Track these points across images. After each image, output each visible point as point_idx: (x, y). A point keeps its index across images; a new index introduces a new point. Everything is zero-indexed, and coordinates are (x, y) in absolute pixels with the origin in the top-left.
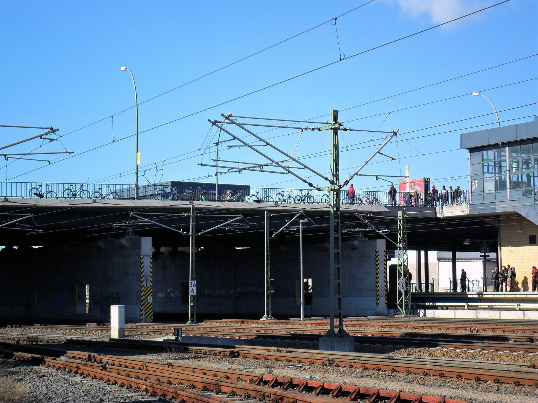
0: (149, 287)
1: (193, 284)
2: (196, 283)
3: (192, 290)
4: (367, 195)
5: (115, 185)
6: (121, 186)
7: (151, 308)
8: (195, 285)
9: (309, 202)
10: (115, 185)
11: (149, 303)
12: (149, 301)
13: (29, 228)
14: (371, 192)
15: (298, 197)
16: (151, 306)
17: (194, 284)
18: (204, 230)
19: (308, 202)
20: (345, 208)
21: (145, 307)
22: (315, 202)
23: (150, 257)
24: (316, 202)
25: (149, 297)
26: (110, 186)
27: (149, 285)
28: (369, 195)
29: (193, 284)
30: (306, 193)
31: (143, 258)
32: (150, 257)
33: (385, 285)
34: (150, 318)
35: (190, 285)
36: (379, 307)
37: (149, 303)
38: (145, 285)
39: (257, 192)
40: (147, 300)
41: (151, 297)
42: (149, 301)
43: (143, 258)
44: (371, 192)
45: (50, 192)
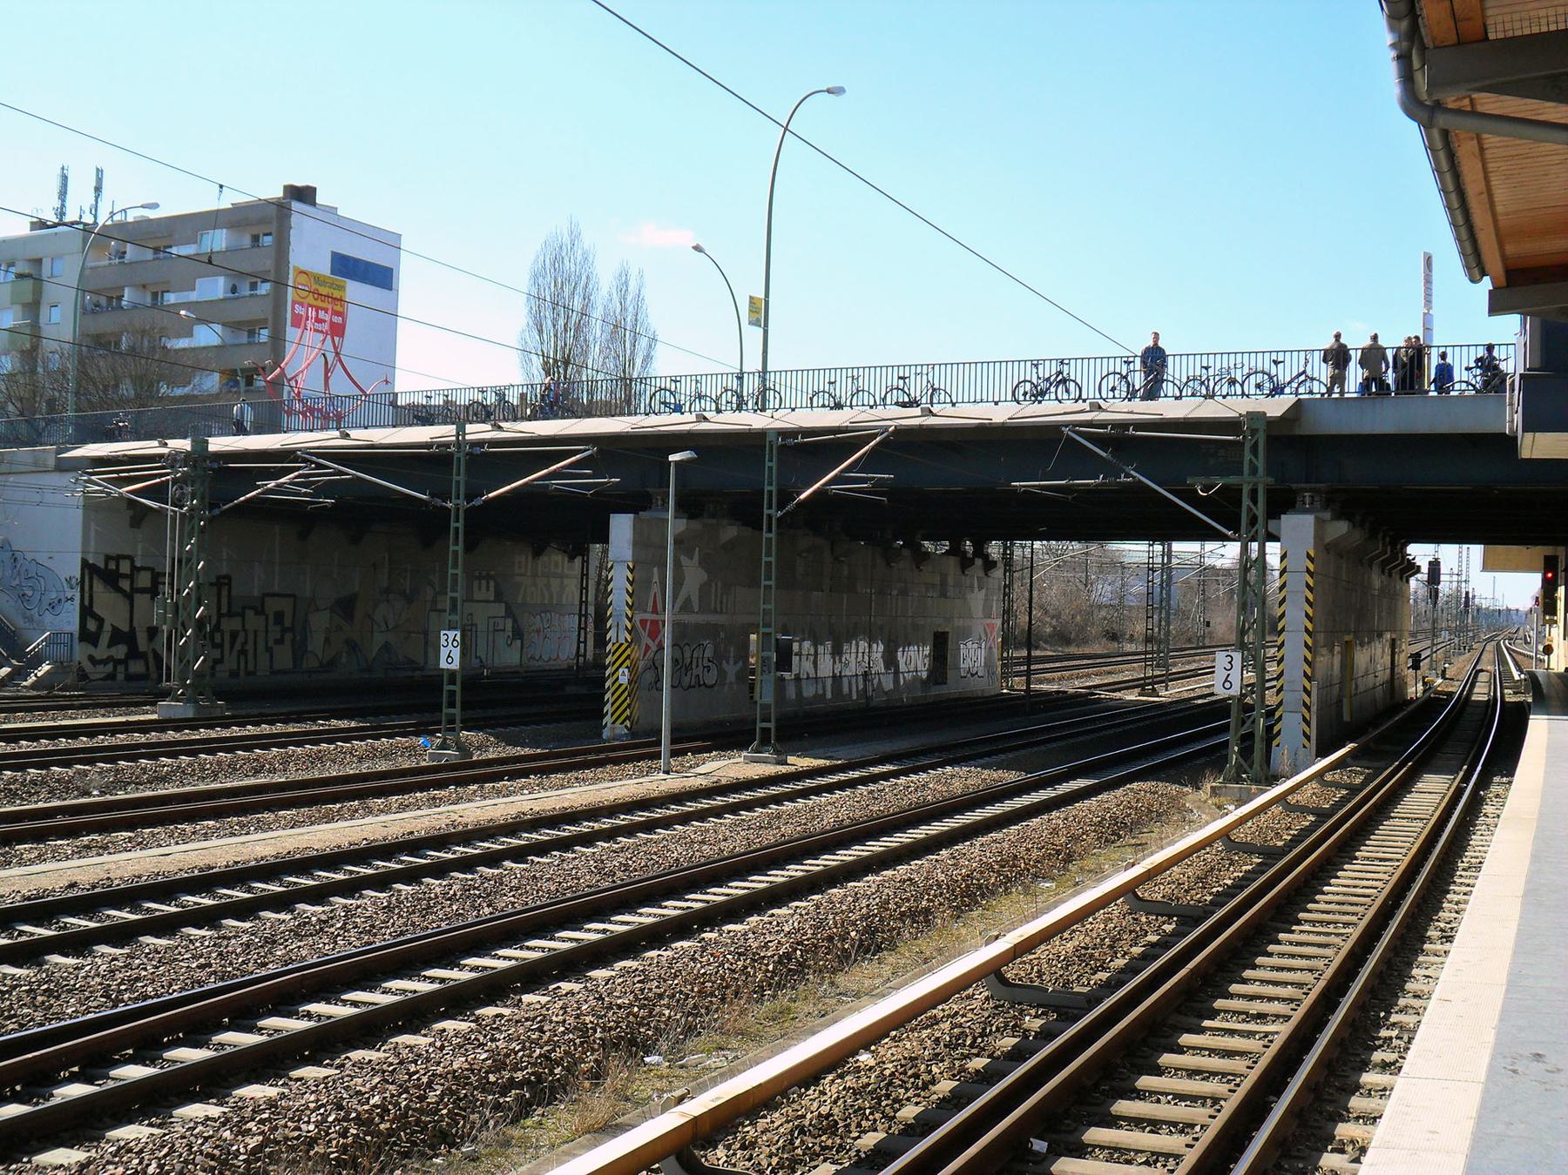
0: (622, 644)
1: (450, 640)
2: (458, 638)
3: (449, 656)
4: (901, 382)
5: (1191, 357)
6: (1112, 360)
7: (626, 699)
8: (455, 644)
9: (1060, 398)
10: (1184, 358)
11: (621, 685)
12: (620, 681)
13: (305, 495)
14: (704, 377)
15: (1028, 385)
16: (626, 693)
17: (454, 640)
18: (224, 505)
19: (1057, 399)
20: (1132, 412)
21: (613, 694)
22: (783, 406)
23: (628, 567)
24: (788, 406)
25: (621, 670)
26: (699, 378)
27: (622, 640)
28: (907, 380)
29: (450, 640)
30: (1054, 372)
31: (612, 567)
32: (628, 567)
33: (1305, 672)
34: (622, 723)
35: (443, 642)
36: (1278, 745)
37: (621, 685)
38: (614, 640)
39: (830, 383)
40: (618, 679)
41: (626, 671)
42: (620, 681)
43: (612, 567)
44: (704, 377)
45: (700, 397)
